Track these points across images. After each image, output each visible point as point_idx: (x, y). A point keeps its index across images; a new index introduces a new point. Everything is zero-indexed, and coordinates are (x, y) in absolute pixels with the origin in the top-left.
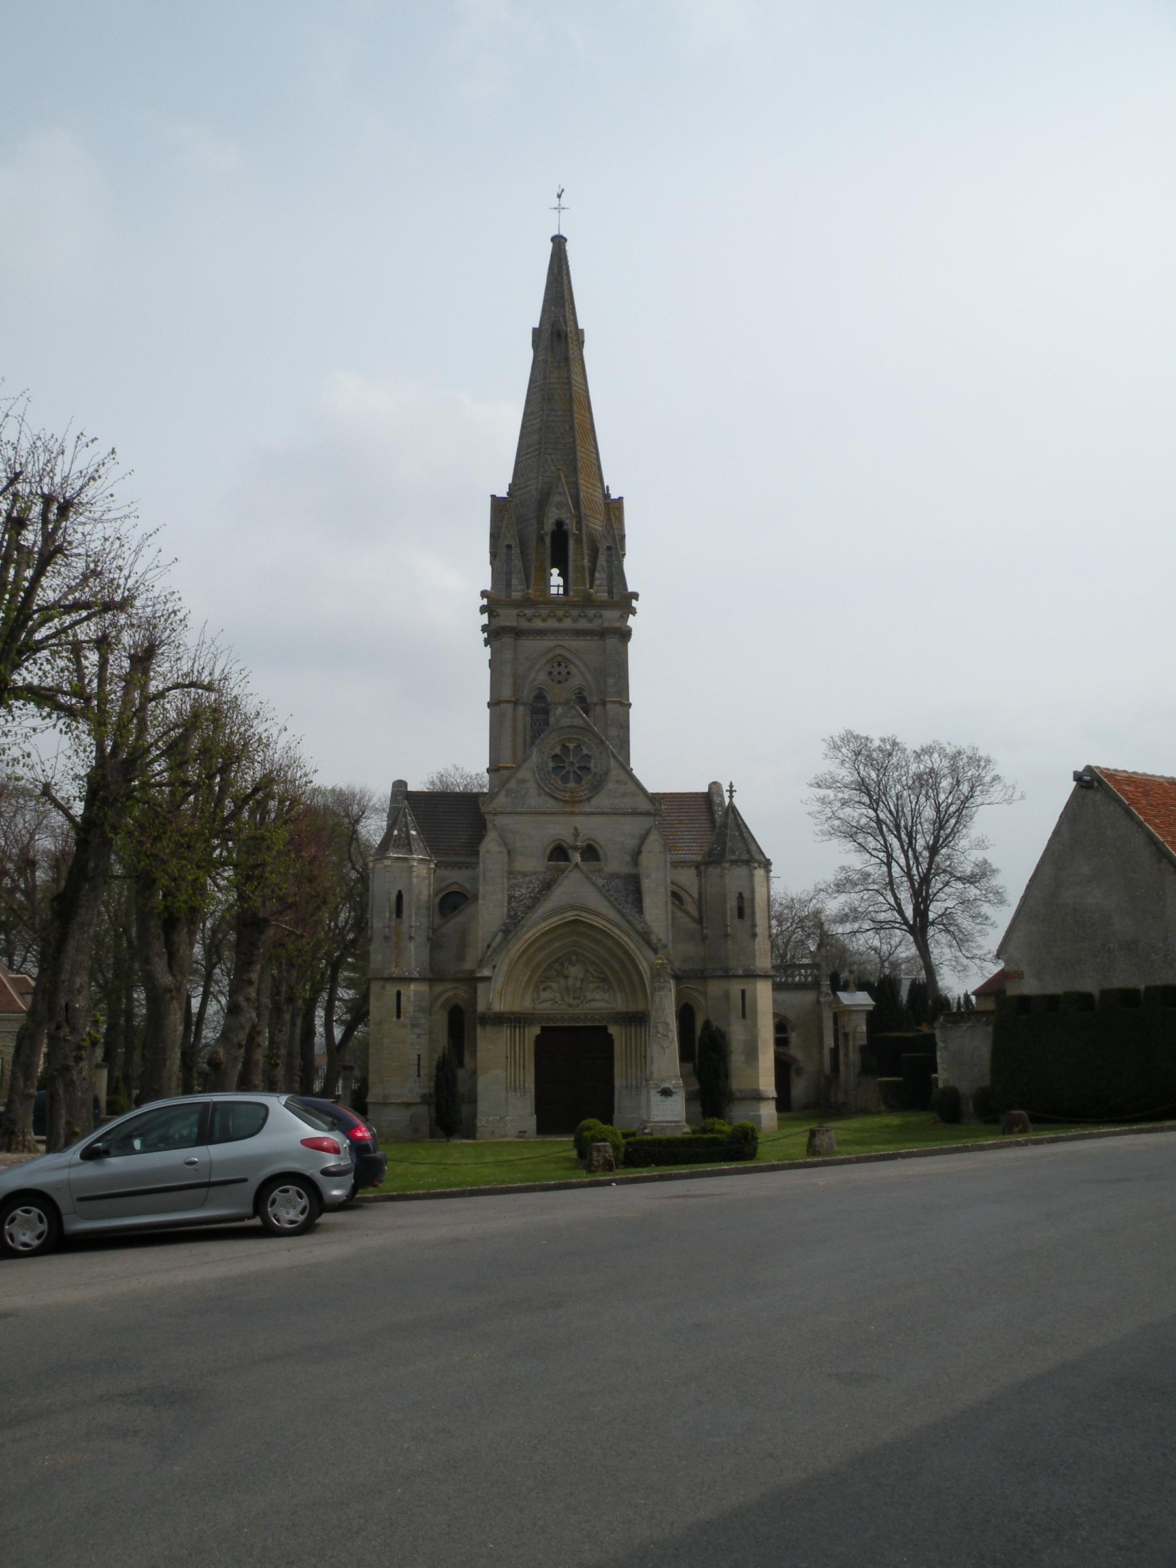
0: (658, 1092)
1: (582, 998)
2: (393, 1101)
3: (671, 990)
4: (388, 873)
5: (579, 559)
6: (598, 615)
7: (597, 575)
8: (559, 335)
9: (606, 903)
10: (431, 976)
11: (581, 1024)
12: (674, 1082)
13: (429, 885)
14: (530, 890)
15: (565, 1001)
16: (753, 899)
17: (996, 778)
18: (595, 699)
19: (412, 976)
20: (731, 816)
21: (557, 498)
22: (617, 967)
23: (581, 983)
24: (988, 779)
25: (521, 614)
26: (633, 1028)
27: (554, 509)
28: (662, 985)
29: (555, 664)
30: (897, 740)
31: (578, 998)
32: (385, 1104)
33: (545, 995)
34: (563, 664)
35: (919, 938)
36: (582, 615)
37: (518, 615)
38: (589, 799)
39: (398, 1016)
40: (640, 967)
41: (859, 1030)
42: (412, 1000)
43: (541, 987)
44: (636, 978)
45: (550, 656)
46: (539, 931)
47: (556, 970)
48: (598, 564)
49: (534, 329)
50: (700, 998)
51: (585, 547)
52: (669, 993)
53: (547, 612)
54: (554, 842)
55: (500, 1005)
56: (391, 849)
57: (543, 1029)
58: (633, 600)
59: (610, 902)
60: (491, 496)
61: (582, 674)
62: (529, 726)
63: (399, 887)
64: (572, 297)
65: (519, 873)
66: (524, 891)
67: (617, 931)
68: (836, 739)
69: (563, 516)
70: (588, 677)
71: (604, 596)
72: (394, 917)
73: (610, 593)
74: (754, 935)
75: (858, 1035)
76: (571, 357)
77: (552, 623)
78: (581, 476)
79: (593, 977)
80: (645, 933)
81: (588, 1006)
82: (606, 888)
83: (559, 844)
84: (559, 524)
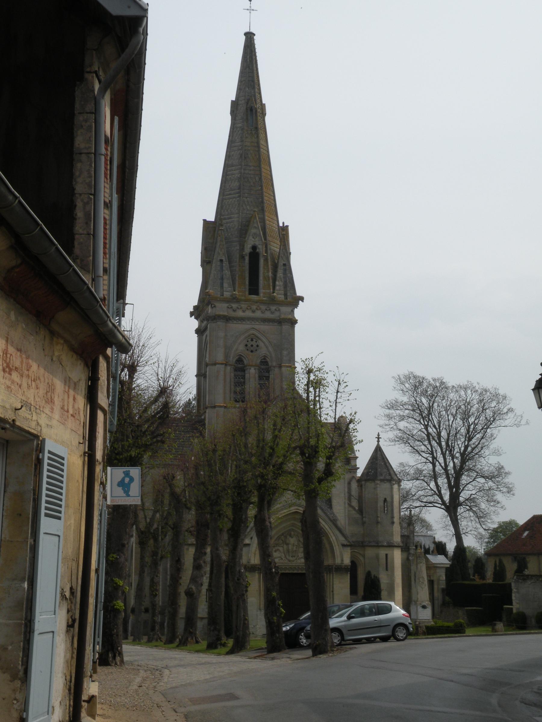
5: (266, 272)
6: (277, 309)
7: (277, 283)
8: (251, 110)
15: (287, 558)
16: (392, 502)
17: (510, 410)
18: (274, 364)
20: (379, 453)
21: (253, 231)
24: (505, 410)
25: (230, 307)
27: (251, 238)
29: (250, 340)
30: (444, 381)
31: (294, 556)
34: (254, 340)
35: (453, 514)
36: (268, 309)
37: (228, 307)
41: (441, 578)
45: (247, 334)
47: (282, 540)
48: (278, 275)
49: (232, 101)
50: (362, 558)
51: (270, 263)
53: (246, 306)
55: (255, 560)
58: (300, 301)
60: (203, 220)
61: (267, 347)
62: (233, 380)
64: (259, 81)
68: (402, 377)
69: (257, 243)
70: (271, 349)
71: (281, 297)
73: (286, 295)
74: (393, 523)
75: (441, 582)
76: (259, 126)
77: (249, 314)
78: (266, 214)
80: (334, 520)
81: (299, 561)
84: (254, 248)
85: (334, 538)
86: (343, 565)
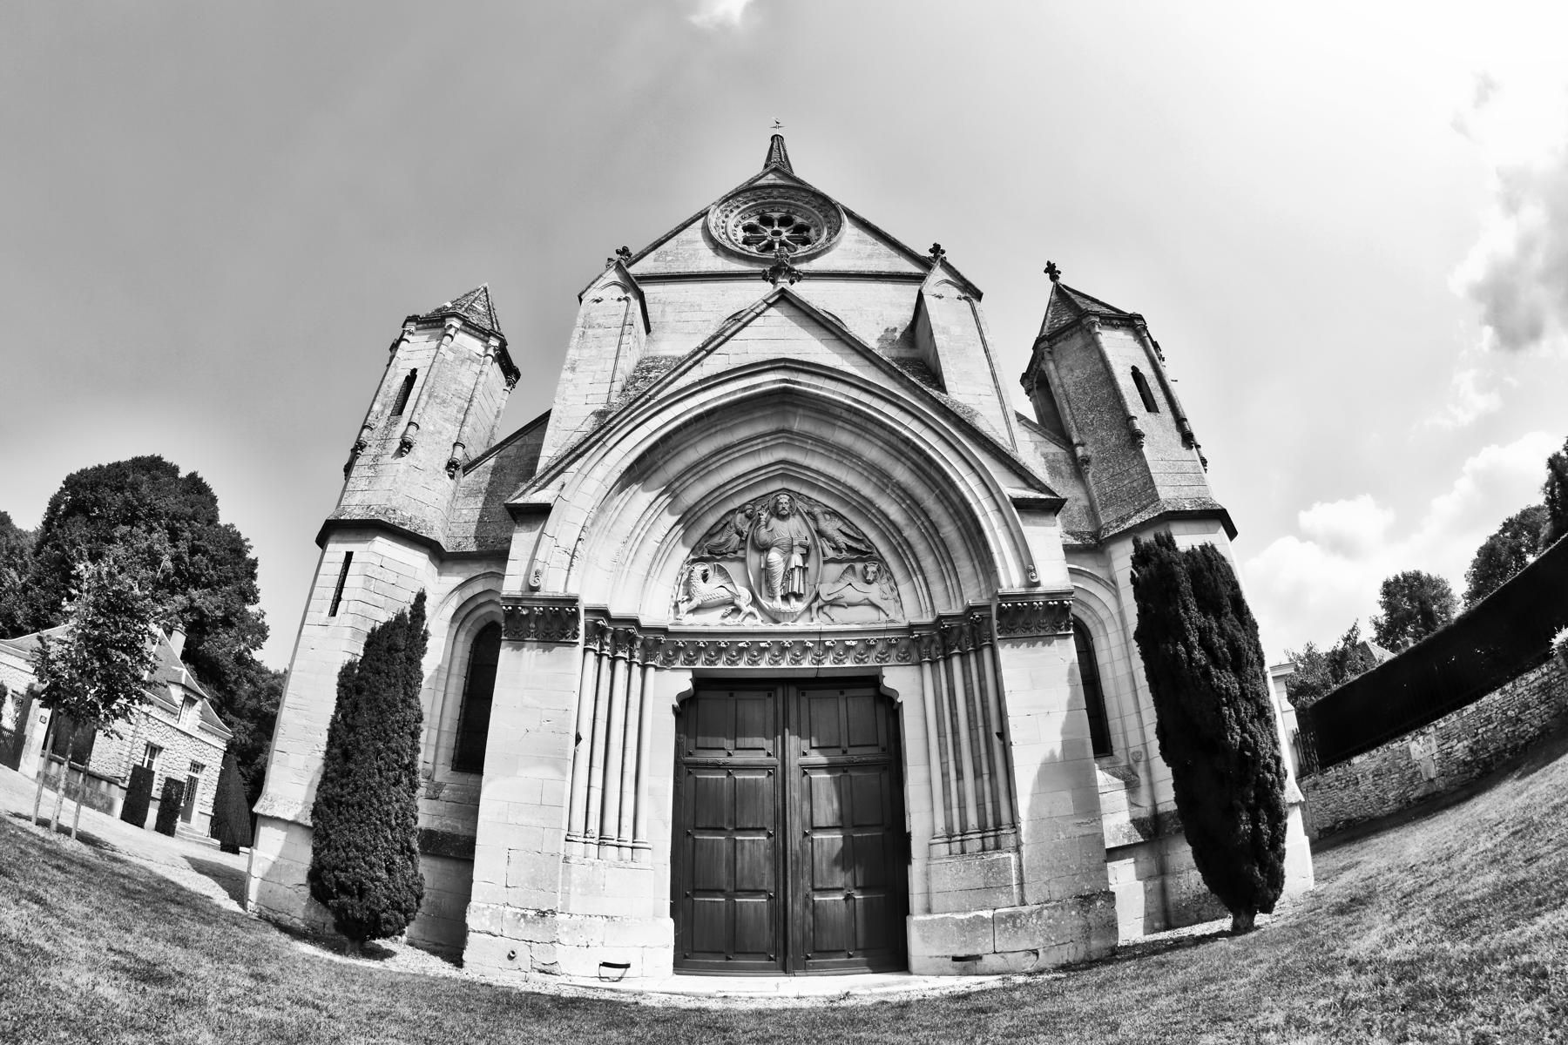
15: (761, 608)
22: (895, 512)
26: (956, 663)
33: (711, 589)
47: (740, 533)
57: (700, 681)
79: (837, 549)
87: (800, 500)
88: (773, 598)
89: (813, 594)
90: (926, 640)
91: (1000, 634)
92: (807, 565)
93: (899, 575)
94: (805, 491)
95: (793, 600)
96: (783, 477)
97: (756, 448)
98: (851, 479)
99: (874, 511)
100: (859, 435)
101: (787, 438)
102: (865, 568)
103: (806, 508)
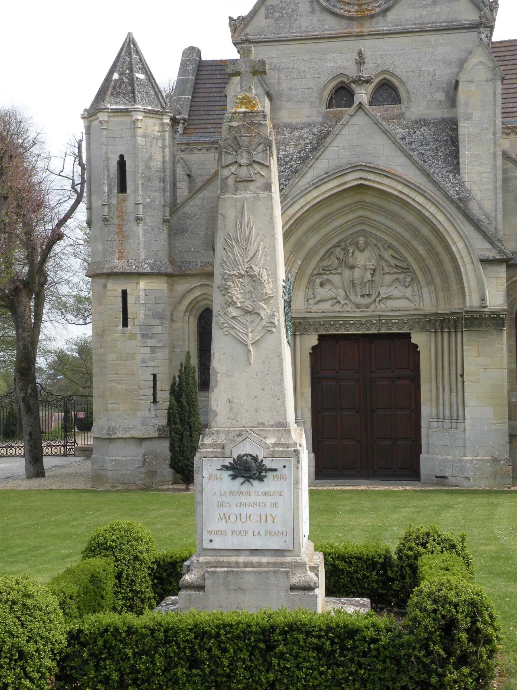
0: (225, 468)
1: (373, 297)
2: (120, 436)
3: (268, 187)
4: (105, 132)
9: (403, 159)
10: (169, 270)
11: (373, 331)
12: (270, 441)
13: (163, 148)
14: (299, 148)
15: (350, 301)
19: (141, 271)
23: (373, 275)
28: (244, 172)
31: (368, 295)
32: (110, 440)
33: (322, 292)
38: (385, 12)
39: (125, 324)
40: (454, 249)
42: (142, 301)
43: (318, 281)
44: (448, 266)
46: (308, 203)
47: (338, 259)
52: (263, 195)
54: (334, 78)
56: (107, 99)
57: (321, 337)
59: (409, 157)
63: (121, 150)
65: (286, 125)
66: (291, 150)
67: (419, 199)
72: (115, 191)
81: (382, 305)
82: (408, 140)
83: (342, 82)
85: (461, 245)
86: (487, 309)
87: (371, 237)
88: (357, 296)
89: (377, 293)
90: (433, 321)
91: (465, 328)
92: (374, 279)
93: (423, 283)
94: (374, 231)
95: (366, 297)
96: (361, 223)
97: (345, 212)
98: (399, 229)
99: (411, 247)
100: (402, 208)
101: (363, 205)
102: (405, 278)
103: (374, 242)
